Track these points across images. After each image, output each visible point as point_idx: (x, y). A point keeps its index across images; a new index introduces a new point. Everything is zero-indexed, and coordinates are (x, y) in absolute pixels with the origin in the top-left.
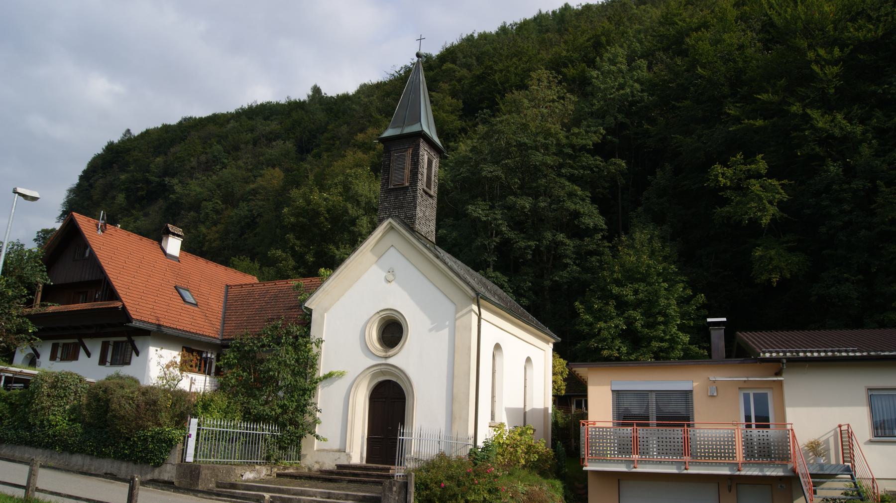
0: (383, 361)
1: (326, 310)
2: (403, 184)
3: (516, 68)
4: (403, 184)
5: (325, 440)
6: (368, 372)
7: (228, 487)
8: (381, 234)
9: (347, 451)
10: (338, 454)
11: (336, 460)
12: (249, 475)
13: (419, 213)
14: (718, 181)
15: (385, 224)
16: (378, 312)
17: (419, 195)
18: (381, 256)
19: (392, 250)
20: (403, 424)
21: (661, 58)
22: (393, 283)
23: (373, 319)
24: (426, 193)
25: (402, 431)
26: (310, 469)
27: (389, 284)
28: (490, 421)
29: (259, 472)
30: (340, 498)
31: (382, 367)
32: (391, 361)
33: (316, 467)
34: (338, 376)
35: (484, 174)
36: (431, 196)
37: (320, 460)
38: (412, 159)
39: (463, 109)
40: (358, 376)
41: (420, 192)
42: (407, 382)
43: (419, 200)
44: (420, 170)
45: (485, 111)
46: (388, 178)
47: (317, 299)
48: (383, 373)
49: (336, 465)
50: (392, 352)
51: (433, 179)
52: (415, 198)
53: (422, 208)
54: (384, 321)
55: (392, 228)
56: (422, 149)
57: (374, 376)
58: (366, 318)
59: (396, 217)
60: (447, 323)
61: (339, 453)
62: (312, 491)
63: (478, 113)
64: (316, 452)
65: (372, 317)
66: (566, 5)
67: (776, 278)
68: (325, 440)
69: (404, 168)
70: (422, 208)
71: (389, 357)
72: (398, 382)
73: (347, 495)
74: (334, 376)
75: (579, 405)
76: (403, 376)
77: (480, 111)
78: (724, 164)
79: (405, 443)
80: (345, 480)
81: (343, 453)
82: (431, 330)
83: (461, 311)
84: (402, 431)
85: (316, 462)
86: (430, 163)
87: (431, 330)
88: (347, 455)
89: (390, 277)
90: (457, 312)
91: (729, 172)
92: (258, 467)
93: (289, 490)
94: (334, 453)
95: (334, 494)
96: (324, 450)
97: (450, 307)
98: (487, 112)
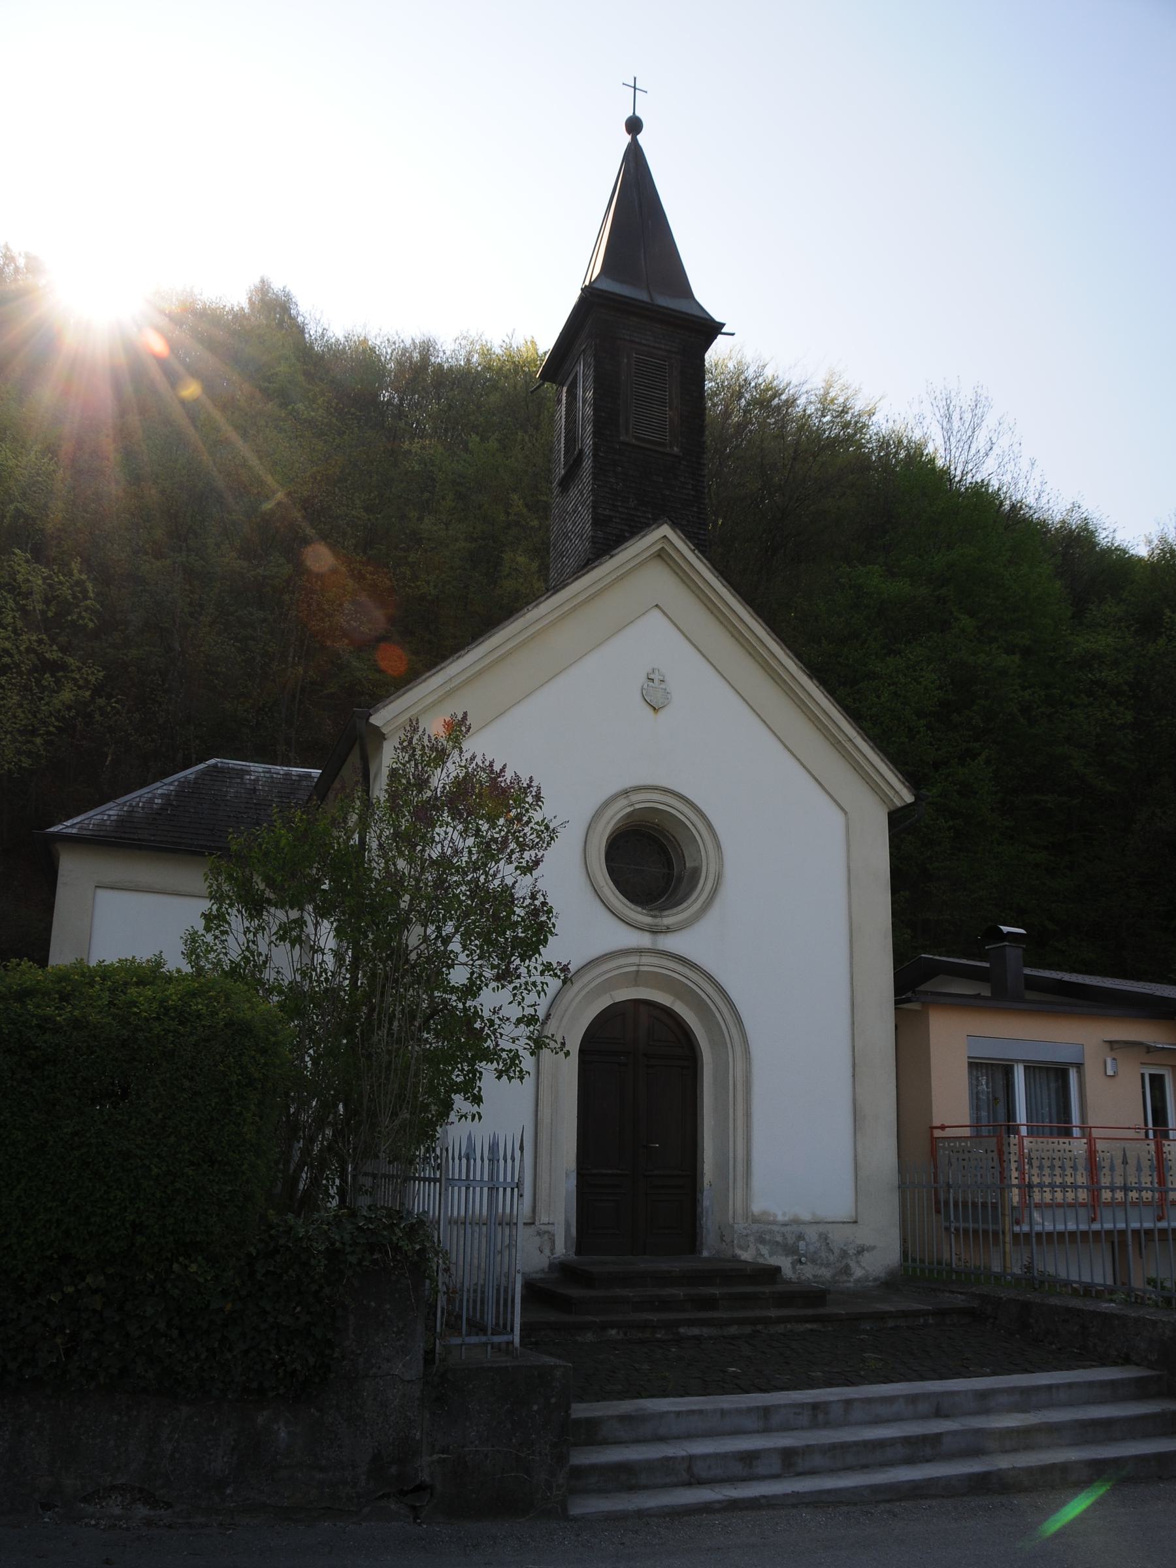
16: (626, 793)
31: (645, 960)
32: (671, 943)
50: (669, 920)
71: (668, 930)
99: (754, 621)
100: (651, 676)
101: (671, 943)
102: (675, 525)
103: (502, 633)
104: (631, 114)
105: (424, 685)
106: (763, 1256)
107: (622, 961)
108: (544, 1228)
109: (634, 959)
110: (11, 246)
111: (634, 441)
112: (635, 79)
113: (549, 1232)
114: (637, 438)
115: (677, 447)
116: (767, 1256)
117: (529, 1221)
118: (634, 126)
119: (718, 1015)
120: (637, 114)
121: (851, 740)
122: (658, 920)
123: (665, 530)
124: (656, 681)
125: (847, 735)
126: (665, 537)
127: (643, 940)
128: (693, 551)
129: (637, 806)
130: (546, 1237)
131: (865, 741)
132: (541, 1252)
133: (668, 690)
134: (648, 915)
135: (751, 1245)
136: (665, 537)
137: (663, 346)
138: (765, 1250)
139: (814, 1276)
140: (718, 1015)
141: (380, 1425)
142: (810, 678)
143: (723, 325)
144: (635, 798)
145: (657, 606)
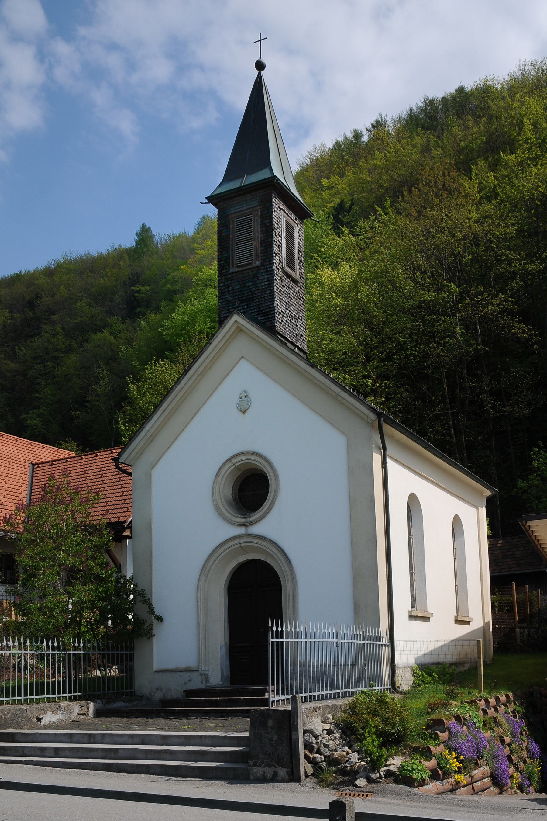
2: (251, 264)
11: (185, 684)
12: (49, 718)
13: (279, 305)
16: (229, 460)
17: (276, 277)
20: (278, 617)
24: (288, 276)
25: (275, 629)
28: (410, 608)
29: (69, 711)
31: (243, 540)
32: (256, 529)
36: (295, 281)
38: (263, 224)
41: (277, 274)
43: (278, 284)
44: (276, 239)
48: (244, 549)
49: (184, 691)
51: (297, 255)
52: (271, 282)
53: (284, 298)
54: (239, 473)
56: (275, 207)
59: (246, 314)
61: (188, 674)
70: (284, 298)
71: (252, 523)
72: (269, 561)
75: (495, 613)
76: (274, 550)
79: (287, 648)
84: (275, 629)
85: (157, 689)
86: (290, 229)
88: (201, 675)
92: (64, 704)
94: (181, 674)
101: (256, 529)
103: (166, 402)
107: (232, 543)
108: (203, 672)
109: (238, 541)
110: (146, 224)
111: (236, 269)
113: (204, 674)
114: (238, 267)
117: (197, 669)
118: (260, 66)
122: (248, 519)
127: (242, 531)
130: (203, 676)
132: (202, 683)
134: (243, 518)
144: (234, 461)
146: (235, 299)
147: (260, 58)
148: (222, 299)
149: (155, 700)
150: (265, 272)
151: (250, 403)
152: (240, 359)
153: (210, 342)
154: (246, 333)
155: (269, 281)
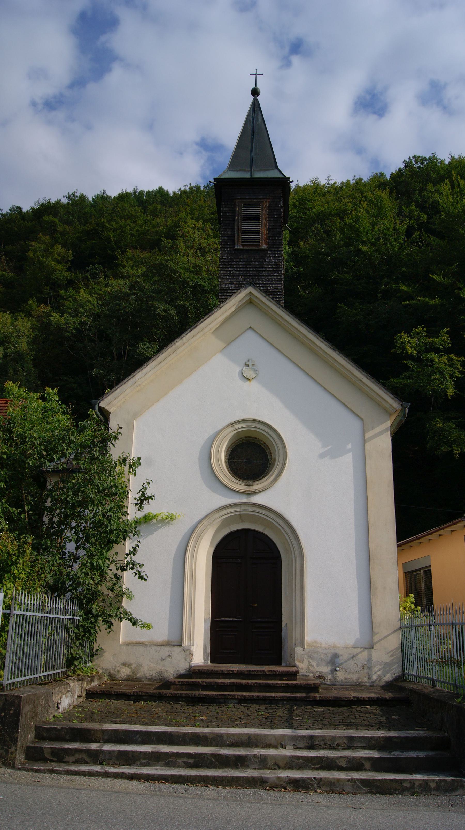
0: (244, 499)
1: (136, 415)
2: (259, 246)
3: (131, 230)
4: (259, 246)
5: (147, 626)
6: (217, 515)
7: (67, 738)
8: (233, 309)
9: (185, 643)
10: (166, 651)
14: (404, 349)
15: (242, 295)
16: (232, 424)
18: (230, 343)
19: (250, 333)
21: (318, 230)
22: (253, 383)
23: (223, 434)
26: (111, 677)
27: (248, 382)
30: (338, 745)
31: (243, 508)
32: (257, 499)
33: (125, 672)
34: (162, 520)
35: (158, 310)
37: (132, 661)
39: (72, 261)
40: (200, 521)
42: (289, 532)
45: (97, 266)
46: (233, 235)
47: (121, 397)
48: (241, 518)
50: (257, 486)
55: (250, 302)
57: (226, 522)
58: (212, 431)
60: (349, 446)
61: (168, 649)
62: (275, 736)
63: (89, 267)
64: (124, 648)
65: (221, 431)
66: (160, 188)
67: (457, 450)
68: (147, 626)
69: (258, 224)
71: (256, 493)
72: (268, 532)
73: (351, 739)
74: (154, 521)
77: (91, 265)
78: (408, 332)
80: (233, 698)
81: (177, 649)
82: (322, 456)
83: (373, 428)
85: (124, 664)
87: (322, 456)
89: (249, 373)
90: (364, 432)
91: (414, 342)
93: (221, 736)
94: (158, 648)
95: (323, 738)
96: (138, 644)
97: (356, 424)
98: (98, 267)
99: (301, 327)
100: (247, 363)
102: (254, 286)
104: (254, 86)
105: (125, 385)
106: (312, 666)
112: (256, 70)
115: (266, 245)
116: (315, 666)
118: (255, 92)
119: (286, 535)
120: (258, 86)
121: (360, 380)
123: (251, 289)
124: (250, 366)
125: (358, 378)
126: (250, 292)
128: (265, 297)
129: (239, 430)
131: (368, 379)
133: (257, 369)
135: (305, 660)
136: (250, 292)
137: (247, 197)
138: (314, 663)
139: (345, 679)
140: (286, 535)
141: (278, 820)
142: (334, 350)
143: (289, 178)
145: (250, 328)
146: (239, 273)
147: (256, 86)
148: (225, 271)
149: (121, 677)
150: (272, 256)
151: (257, 372)
152: (248, 329)
153: (221, 306)
154: (256, 306)
155: (277, 265)
